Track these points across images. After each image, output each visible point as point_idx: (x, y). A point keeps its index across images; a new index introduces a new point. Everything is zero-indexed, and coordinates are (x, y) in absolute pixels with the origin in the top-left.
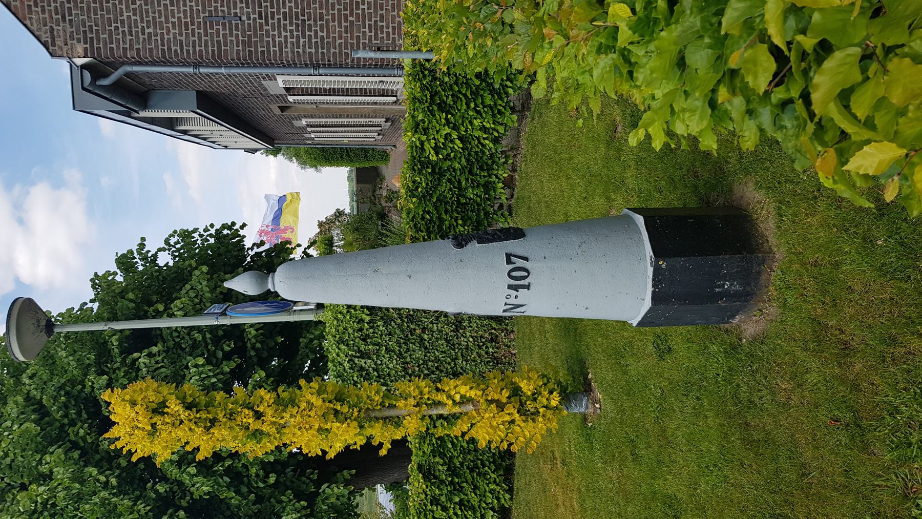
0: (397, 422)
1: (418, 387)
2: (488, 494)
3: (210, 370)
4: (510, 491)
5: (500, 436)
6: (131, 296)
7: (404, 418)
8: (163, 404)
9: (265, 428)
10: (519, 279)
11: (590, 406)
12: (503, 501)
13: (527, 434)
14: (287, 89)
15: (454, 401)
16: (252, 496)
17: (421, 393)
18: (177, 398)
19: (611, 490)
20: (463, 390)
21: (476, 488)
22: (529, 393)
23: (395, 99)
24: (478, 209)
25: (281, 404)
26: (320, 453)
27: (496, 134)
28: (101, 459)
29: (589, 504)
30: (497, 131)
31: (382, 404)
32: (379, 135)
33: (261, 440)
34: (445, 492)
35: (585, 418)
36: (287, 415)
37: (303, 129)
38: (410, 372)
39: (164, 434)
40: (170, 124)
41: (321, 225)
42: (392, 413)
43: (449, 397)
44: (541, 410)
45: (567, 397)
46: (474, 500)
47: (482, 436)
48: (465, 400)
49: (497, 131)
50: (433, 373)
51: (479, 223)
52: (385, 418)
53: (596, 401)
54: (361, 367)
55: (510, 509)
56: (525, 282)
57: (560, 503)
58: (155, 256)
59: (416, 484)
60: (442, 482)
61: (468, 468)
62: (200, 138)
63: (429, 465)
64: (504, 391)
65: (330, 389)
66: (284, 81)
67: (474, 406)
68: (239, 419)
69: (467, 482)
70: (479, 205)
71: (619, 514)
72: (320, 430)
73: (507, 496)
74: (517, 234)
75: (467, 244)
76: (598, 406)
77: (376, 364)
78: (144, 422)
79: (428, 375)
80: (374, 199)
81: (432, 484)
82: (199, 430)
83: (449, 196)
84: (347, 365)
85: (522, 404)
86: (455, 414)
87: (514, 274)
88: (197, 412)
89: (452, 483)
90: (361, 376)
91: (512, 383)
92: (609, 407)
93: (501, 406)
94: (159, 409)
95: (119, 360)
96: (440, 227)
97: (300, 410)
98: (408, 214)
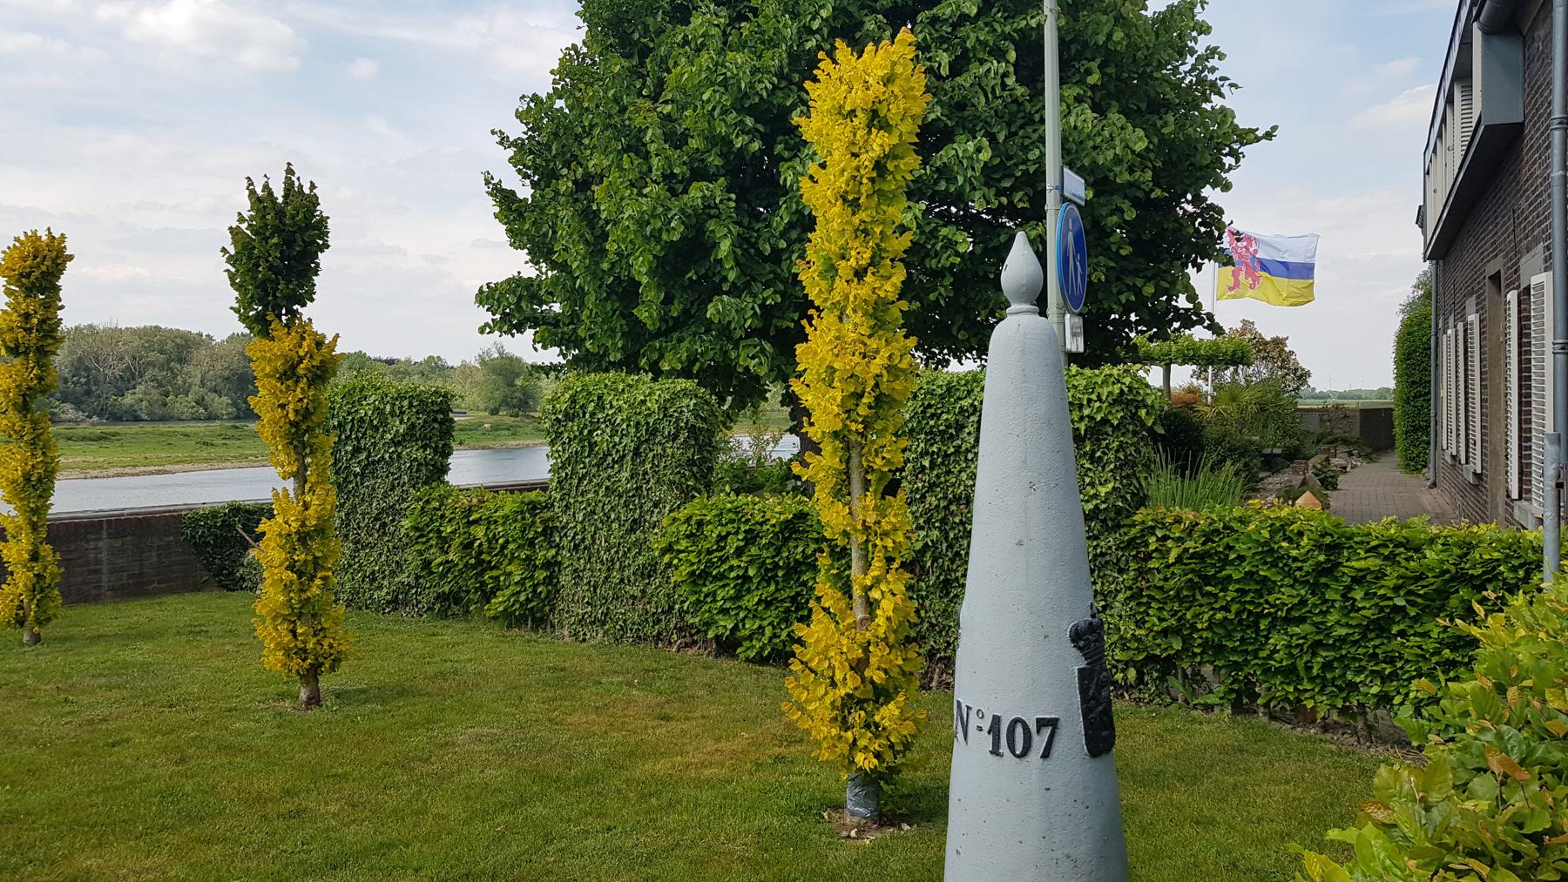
5: (811, 660)
6: (1118, 35)
7: (848, 504)
8: (885, 126)
9: (839, 284)
10: (1011, 737)
11: (856, 819)
12: (747, 644)
13: (811, 707)
14: (1528, 289)
15: (870, 588)
16: (783, 244)
17: (886, 534)
19: (717, 837)
20: (887, 606)
22: (877, 718)
23: (1515, 495)
24: (1246, 652)
25: (877, 311)
26: (800, 368)
27: (1398, 700)
28: (850, 15)
29: (706, 795)
30: (1402, 704)
31: (870, 470)
32: (1453, 457)
33: (824, 278)
35: (838, 807)
36: (858, 318)
37: (1462, 317)
38: (953, 508)
39: (838, 130)
40: (1462, 74)
41: (1279, 343)
42: (856, 486)
43: (877, 581)
44: (849, 735)
45: (869, 782)
46: (750, 601)
47: (816, 632)
48: (871, 605)
49: (1402, 704)
50: (950, 546)
51: (1220, 650)
52: (847, 473)
53: (861, 831)
55: (734, 656)
56: (1004, 748)
57: (722, 745)
59: (778, 509)
61: (798, 594)
62: (1440, 126)
63: (804, 531)
64: (882, 674)
65: (897, 386)
66: (1541, 286)
68: (856, 244)
69: (777, 590)
70: (1255, 652)
72: (832, 370)
74: (1100, 737)
75: (1080, 648)
76: (853, 834)
78: (858, 98)
79: (946, 538)
80: (1330, 441)
81: (776, 534)
82: (841, 182)
83: (1271, 599)
84: (965, 403)
85: (861, 703)
87: (1019, 730)
88: (872, 180)
89: (776, 566)
90: (948, 427)
92: (844, 855)
93: (858, 666)
94: (876, 120)
95: (1008, 29)
96: (1208, 580)
98: (1241, 520)
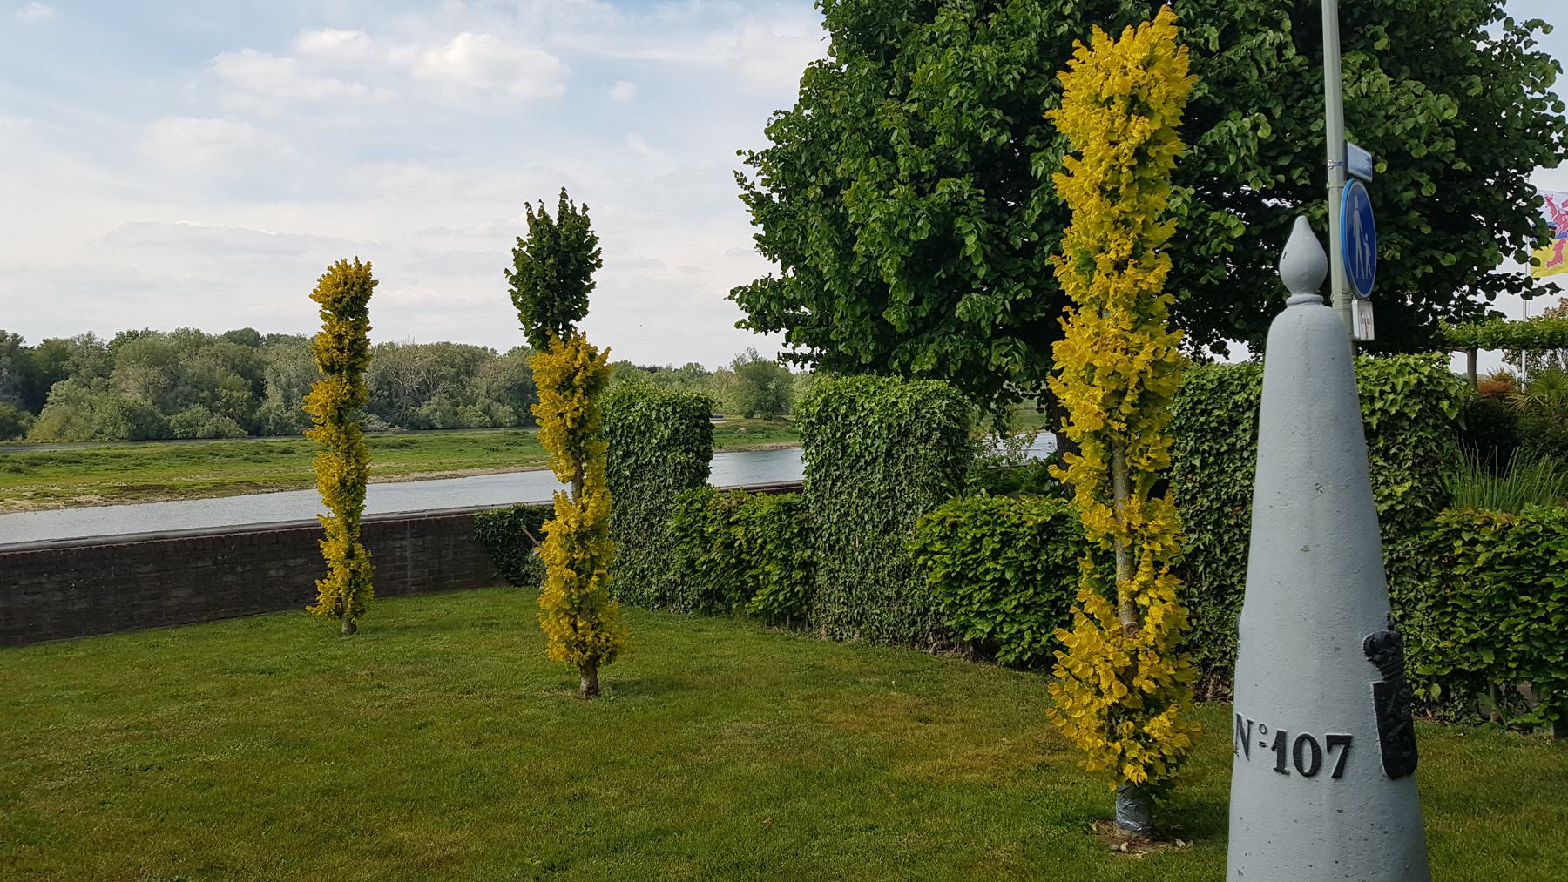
0: (1104, 493)
1: (1164, 532)
2: (1016, 627)
3: (1248, 149)
4: (1020, 665)
5: (1074, 666)
8: (1146, 111)
9: (1098, 278)
10: (1295, 754)
11: (1126, 833)
13: (1077, 715)
15: (1138, 594)
17: (1153, 538)
18: (1155, 133)
19: (981, 843)
20: (1156, 613)
21: (1026, 608)
22: (1146, 729)
26: (1057, 367)
29: (968, 800)
31: (1134, 470)
33: (1082, 273)
34: (1022, 557)
35: (1107, 818)
36: (1119, 312)
38: (1227, 509)
39: (1095, 118)
42: (1120, 488)
43: (1145, 587)
44: (1117, 745)
45: (1140, 795)
46: (1008, 604)
48: (1138, 613)
50: (1225, 550)
52: (1110, 474)
54: (1237, 423)
55: (993, 660)
57: (983, 750)
58: (1499, 15)
60: (1036, 555)
61: (1058, 598)
63: (1064, 534)
64: (1152, 684)
65: (1163, 382)
67: (1129, 627)
69: (1036, 594)
71: (941, 847)
72: (1091, 368)
73: (1011, 658)
76: (1123, 847)
77: (1243, 449)
78: (1115, 84)
81: (1034, 537)
85: (1129, 713)
86: (1116, 593)
87: (1307, 748)
88: (1132, 168)
89: (1034, 569)
90: (1221, 423)
91: (1168, 701)
93: (1126, 676)
97: (1128, 335)
